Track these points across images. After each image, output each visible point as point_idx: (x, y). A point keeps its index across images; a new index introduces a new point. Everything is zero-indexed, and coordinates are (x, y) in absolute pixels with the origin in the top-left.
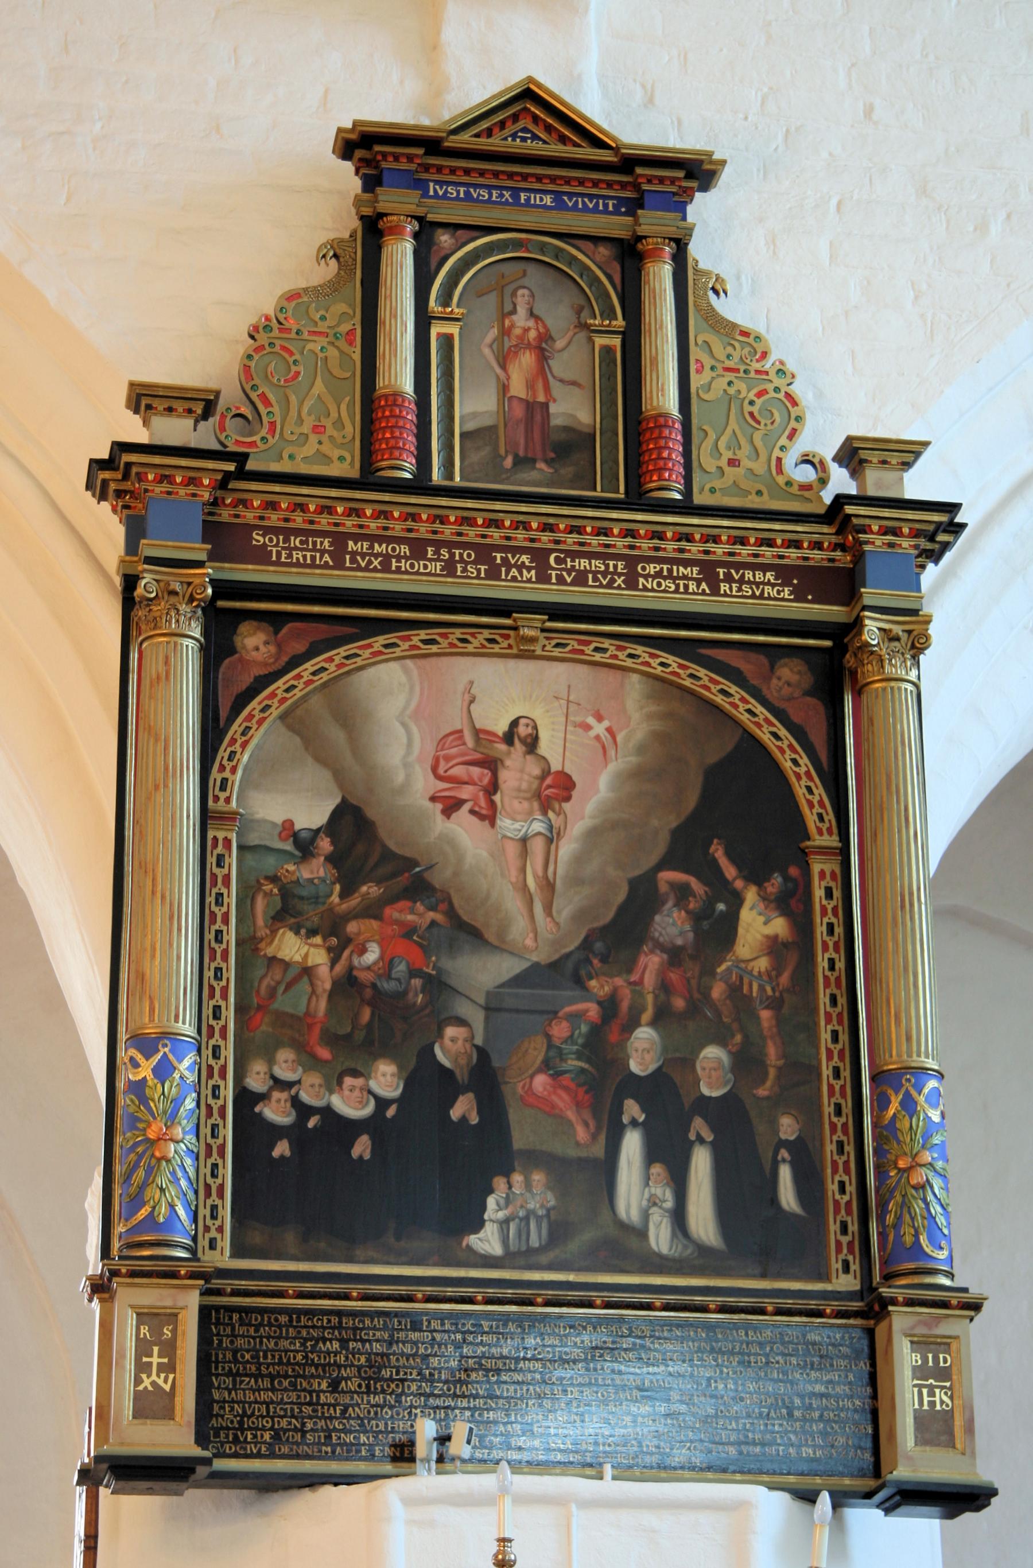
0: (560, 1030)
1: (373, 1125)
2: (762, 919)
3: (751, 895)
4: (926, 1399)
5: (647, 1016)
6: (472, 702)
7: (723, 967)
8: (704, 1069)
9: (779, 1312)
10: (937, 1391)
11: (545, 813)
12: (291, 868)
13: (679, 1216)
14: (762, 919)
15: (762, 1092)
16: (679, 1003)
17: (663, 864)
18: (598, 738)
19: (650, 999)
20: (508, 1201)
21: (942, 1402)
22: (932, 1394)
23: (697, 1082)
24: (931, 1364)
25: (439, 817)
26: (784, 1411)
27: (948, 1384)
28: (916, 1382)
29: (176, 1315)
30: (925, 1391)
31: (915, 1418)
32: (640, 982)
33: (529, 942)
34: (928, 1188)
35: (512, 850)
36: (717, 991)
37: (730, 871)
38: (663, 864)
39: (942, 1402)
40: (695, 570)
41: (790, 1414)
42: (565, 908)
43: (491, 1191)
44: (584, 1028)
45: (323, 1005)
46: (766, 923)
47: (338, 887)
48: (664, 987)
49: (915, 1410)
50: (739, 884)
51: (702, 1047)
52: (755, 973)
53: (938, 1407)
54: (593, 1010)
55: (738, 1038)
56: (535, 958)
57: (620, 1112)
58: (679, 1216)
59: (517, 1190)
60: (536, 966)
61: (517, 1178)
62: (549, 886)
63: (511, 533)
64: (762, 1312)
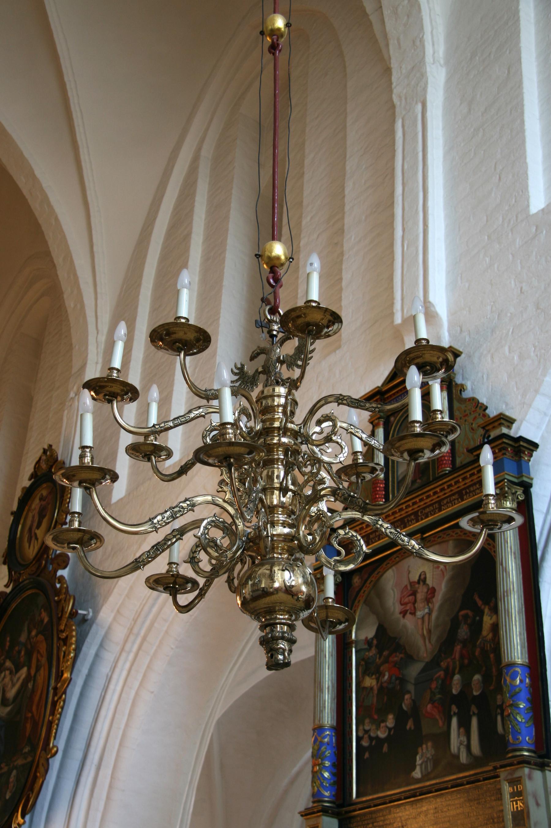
0: (434, 686)
1: (388, 739)
2: (489, 618)
3: (486, 610)
4: (515, 806)
5: (457, 671)
6: (409, 573)
7: (479, 642)
8: (474, 685)
9: (485, 779)
10: (518, 802)
11: (428, 605)
12: (367, 653)
13: (468, 747)
14: (489, 618)
15: (492, 688)
16: (466, 661)
17: (461, 609)
18: (442, 570)
19: (458, 663)
20: (422, 756)
21: (520, 806)
22: (517, 804)
23: (472, 690)
24: (515, 790)
25: (402, 619)
26: (491, 820)
27: (521, 798)
28: (511, 800)
29: (520, 780)
30: (514, 803)
31: (512, 815)
32: (455, 658)
33: (425, 655)
34: (511, 715)
35: (420, 622)
36: (477, 652)
37: (479, 603)
38: (461, 609)
39: (520, 806)
40: (457, 495)
41: (493, 821)
42: (434, 639)
43: (417, 753)
44: (440, 682)
45: (375, 699)
46: (491, 619)
47: (378, 656)
48: (462, 656)
49: (512, 812)
50: (483, 607)
51: (474, 675)
52: (488, 640)
53: (519, 809)
54: (442, 673)
55: (484, 669)
56: (427, 660)
57: (450, 710)
58: (468, 747)
59: (424, 751)
60: (427, 663)
61: (424, 746)
62: (429, 631)
63: (407, 510)
64: (479, 781)
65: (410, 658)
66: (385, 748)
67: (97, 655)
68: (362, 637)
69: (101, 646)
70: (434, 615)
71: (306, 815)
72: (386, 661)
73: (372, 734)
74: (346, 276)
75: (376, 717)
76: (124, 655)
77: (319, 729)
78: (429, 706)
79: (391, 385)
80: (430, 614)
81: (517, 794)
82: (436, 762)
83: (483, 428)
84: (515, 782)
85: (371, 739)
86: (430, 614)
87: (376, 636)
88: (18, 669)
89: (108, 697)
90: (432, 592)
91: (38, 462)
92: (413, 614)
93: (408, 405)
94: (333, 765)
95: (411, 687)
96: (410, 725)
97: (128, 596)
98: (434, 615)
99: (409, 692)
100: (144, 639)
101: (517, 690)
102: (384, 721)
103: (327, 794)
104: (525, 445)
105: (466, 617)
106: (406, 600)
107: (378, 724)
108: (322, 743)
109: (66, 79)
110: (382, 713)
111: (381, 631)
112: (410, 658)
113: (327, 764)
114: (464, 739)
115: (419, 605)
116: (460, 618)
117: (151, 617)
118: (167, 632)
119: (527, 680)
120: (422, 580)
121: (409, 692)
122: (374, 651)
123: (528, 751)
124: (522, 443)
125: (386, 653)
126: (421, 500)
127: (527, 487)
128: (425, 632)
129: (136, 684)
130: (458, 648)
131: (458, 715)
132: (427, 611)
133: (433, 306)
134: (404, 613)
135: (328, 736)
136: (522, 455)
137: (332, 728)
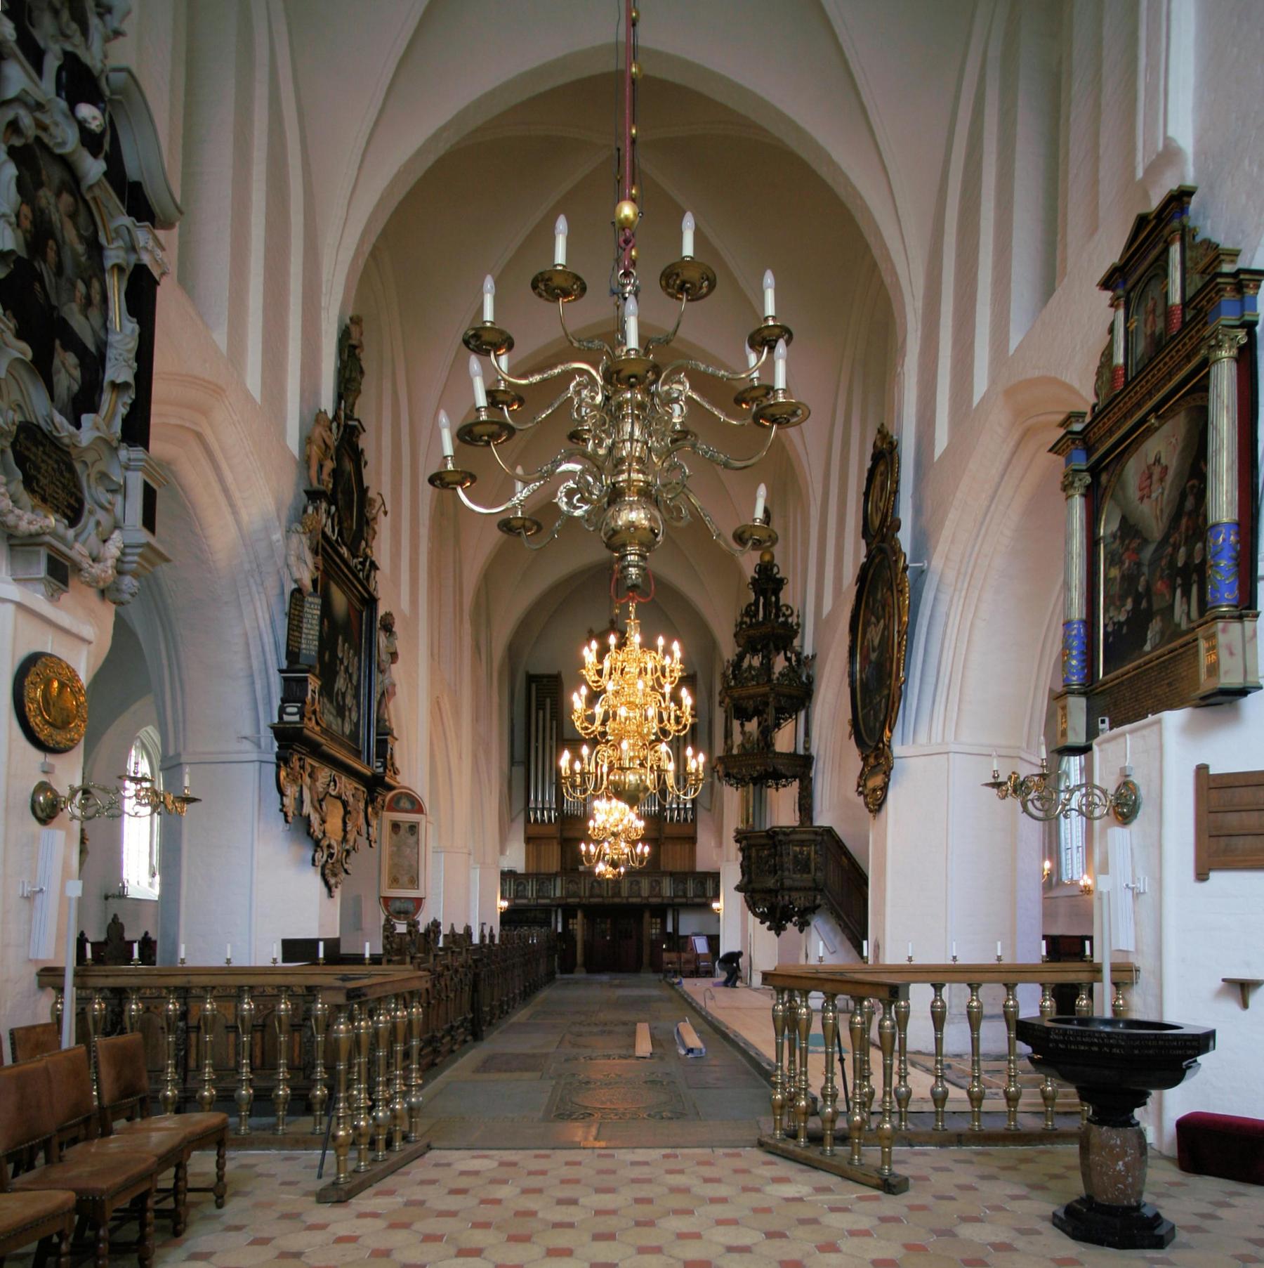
1: (1128, 620)
16: (1190, 532)
38: (1190, 478)
43: (1148, 629)
48: (1187, 529)
62: (1161, 510)
65: (1146, 541)
66: (1125, 630)
67: (935, 598)
68: (1109, 532)
69: (938, 590)
70: (1166, 492)
71: (1057, 698)
72: (1127, 549)
73: (1116, 620)
74: (1103, 141)
75: (1118, 603)
76: (957, 593)
77: (1068, 624)
78: (1159, 583)
79: (1128, 255)
80: (1162, 493)
81: (1212, 648)
82: (1162, 633)
83: (116, 449)
84: (1211, 637)
85: (1114, 624)
86: (1162, 493)
87: (1120, 528)
88: (878, 622)
89: (949, 631)
90: (1165, 469)
91: (875, 443)
92: (1149, 497)
93: (1237, 255)
94: (1082, 653)
95: (1145, 570)
96: (1144, 604)
97: (952, 542)
98: (1166, 492)
99: (1143, 574)
100: (972, 575)
101: (1219, 549)
102: (1124, 605)
103: (1075, 678)
104: (1247, 277)
105: (1193, 486)
106: (1144, 485)
107: (1119, 609)
108: (1069, 636)
109: (841, 40)
110: (1123, 598)
111: (1124, 519)
112: (1146, 541)
113: (1074, 653)
114: (1185, 607)
115: (1154, 487)
116: (1188, 490)
117: (974, 555)
118: (989, 565)
119: (1232, 538)
120: (1158, 460)
121: (1143, 574)
122: (1118, 542)
123: (1227, 606)
124: (1242, 276)
125: (1127, 542)
126: (1153, 376)
127: (1250, 327)
128: (1158, 513)
129: (971, 616)
130: (1184, 521)
131: (1182, 585)
132: (1160, 490)
133: (1175, 141)
134: (1142, 499)
135: (1078, 630)
136: (1245, 290)
137: (1081, 621)
